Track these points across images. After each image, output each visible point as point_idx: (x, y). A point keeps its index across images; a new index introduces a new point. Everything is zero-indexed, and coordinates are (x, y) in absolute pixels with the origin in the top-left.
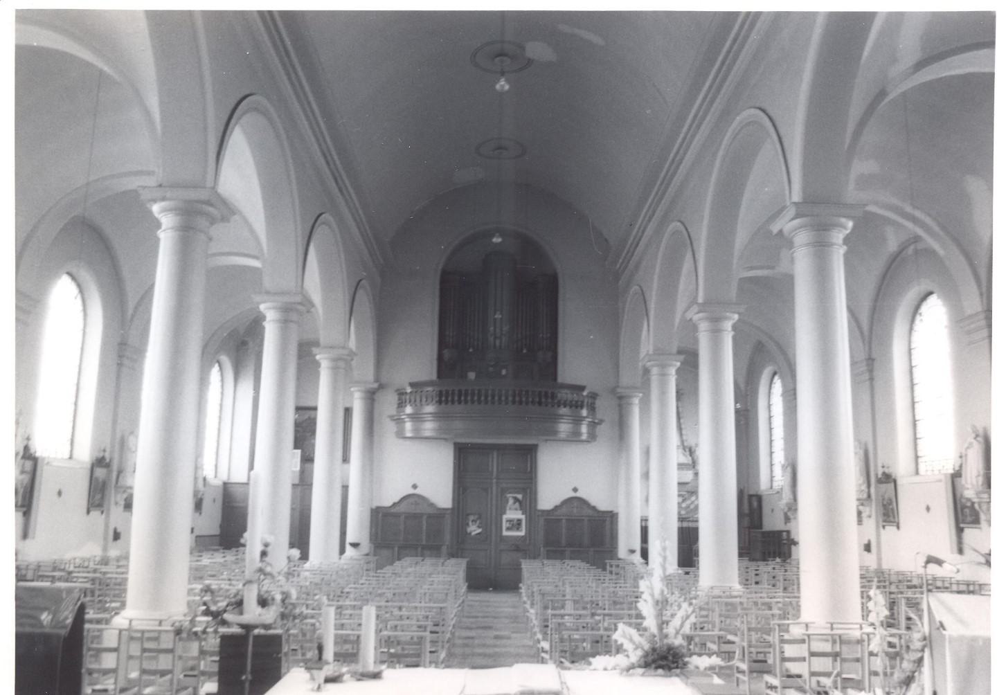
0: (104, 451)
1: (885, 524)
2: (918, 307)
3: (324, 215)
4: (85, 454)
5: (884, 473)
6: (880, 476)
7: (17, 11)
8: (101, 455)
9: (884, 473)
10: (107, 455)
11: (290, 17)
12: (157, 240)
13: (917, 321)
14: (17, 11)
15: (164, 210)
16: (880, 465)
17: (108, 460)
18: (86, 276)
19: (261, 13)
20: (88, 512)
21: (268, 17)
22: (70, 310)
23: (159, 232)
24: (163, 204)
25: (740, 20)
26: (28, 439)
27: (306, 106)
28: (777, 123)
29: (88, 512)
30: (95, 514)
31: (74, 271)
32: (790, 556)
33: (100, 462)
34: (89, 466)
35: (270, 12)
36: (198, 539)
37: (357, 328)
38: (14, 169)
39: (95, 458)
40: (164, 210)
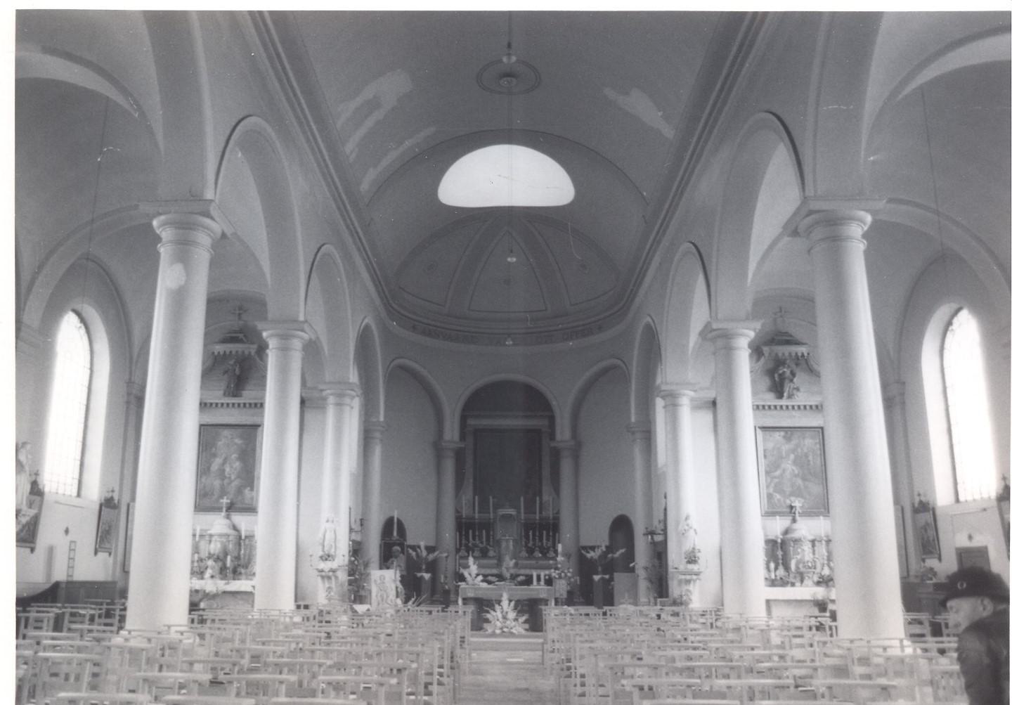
0: (113, 491)
1: (924, 557)
2: (950, 323)
3: (325, 246)
4: (94, 492)
5: (921, 502)
6: (916, 505)
7: (17, 11)
8: (110, 495)
9: (921, 502)
10: (116, 498)
11: (281, 18)
12: (158, 254)
13: (949, 335)
14: (17, 11)
15: (164, 224)
16: (916, 493)
17: (116, 502)
18: (92, 313)
19: (251, 13)
20: (96, 553)
21: (257, 17)
22: (76, 350)
23: (159, 245)
24: (162, 218)
25: (746, 23)
26: (37, 474)
27: (296, 106)
28: (791, 127)
29: (96, 553)
30: (102, 556)
31: (78, 307)
32: (823, 600)
33: (108, 504)
34: (97, 507)
35: (260, 13)
36: (202, 427)
37: (385, 459)
38: (14, 215)
39: (103, 499)
40: (164, 224)
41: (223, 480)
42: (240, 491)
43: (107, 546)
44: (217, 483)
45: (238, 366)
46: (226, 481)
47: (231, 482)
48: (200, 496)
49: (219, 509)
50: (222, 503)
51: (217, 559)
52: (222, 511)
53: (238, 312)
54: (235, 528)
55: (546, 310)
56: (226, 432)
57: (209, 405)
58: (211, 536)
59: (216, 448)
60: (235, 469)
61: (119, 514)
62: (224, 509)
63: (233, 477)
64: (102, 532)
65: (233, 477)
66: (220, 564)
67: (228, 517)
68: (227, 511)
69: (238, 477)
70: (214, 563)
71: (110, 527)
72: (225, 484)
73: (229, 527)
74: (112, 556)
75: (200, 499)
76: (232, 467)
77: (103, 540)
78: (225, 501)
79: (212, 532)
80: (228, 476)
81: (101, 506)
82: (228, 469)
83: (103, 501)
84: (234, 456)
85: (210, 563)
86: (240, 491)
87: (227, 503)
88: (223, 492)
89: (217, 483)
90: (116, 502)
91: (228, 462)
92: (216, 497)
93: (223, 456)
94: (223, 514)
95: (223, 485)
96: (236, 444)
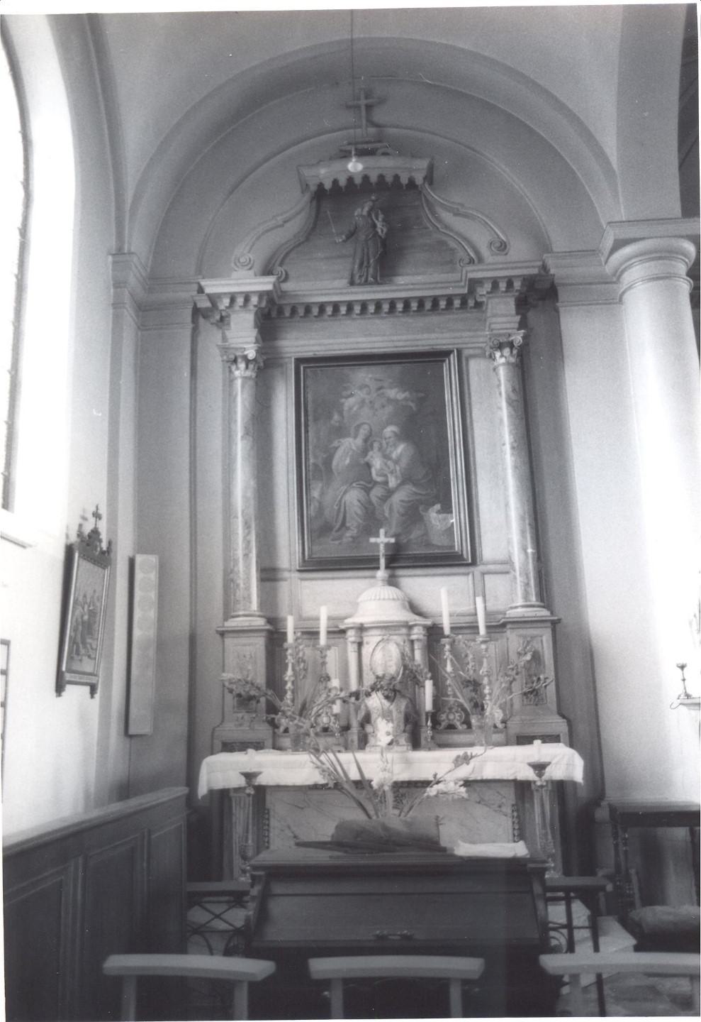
10: (103, 527)
20: (59, 689)
29: (59, 689)
30: (76, 693)
41: (367, 490)
42: (413, 514)
43: (87, 666)
44: (353, 497)
45: (381, 217)
46: (377, 492)
47: (390, 493)
48: (311, 532)
49: (364, 563)
50: (377, 545)
51: (392, 693)
52: (378, 568)
53: (363, 102)
54: (414, 608)
55: (483, 574)
56: (363, 376)
57: (315, 311)
58: (361, 629)
59: (341, 413)
60: (397, 462)
61: (113, 577)
62: (382, 562)
63: (393, 483)
64: (75, 630)
65: (393, 483)
66: (403, 704)
67: (392, 581)
68: (387, 567)
69: (407, 479)
70: (386, 703)
71: (93, 614)
72: (374, 500)
73: (404, 607)
74: (97, 696)
75: (312, 541)
76: (386, 457)
77: (78, 653)
78: (382, 540)
79: (357, 620)
80: (379, 479)
81: (69, 551)
82: (377, 463)
83: (74, 538)
84: (390, 430)
85: (376, 702)
86: (413, 514)
87: (387, 545)
88: (372, 522)
89: (353, 497)
90: (104, 546)
91: (376, 445)
92: (353, 532)
93: (363, 432)
94: (382, 573)
95: (370, 502)
96: (389, 400)
